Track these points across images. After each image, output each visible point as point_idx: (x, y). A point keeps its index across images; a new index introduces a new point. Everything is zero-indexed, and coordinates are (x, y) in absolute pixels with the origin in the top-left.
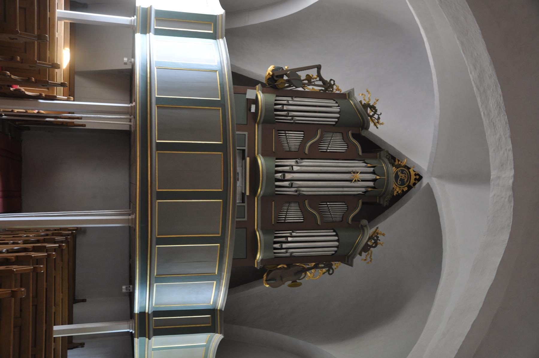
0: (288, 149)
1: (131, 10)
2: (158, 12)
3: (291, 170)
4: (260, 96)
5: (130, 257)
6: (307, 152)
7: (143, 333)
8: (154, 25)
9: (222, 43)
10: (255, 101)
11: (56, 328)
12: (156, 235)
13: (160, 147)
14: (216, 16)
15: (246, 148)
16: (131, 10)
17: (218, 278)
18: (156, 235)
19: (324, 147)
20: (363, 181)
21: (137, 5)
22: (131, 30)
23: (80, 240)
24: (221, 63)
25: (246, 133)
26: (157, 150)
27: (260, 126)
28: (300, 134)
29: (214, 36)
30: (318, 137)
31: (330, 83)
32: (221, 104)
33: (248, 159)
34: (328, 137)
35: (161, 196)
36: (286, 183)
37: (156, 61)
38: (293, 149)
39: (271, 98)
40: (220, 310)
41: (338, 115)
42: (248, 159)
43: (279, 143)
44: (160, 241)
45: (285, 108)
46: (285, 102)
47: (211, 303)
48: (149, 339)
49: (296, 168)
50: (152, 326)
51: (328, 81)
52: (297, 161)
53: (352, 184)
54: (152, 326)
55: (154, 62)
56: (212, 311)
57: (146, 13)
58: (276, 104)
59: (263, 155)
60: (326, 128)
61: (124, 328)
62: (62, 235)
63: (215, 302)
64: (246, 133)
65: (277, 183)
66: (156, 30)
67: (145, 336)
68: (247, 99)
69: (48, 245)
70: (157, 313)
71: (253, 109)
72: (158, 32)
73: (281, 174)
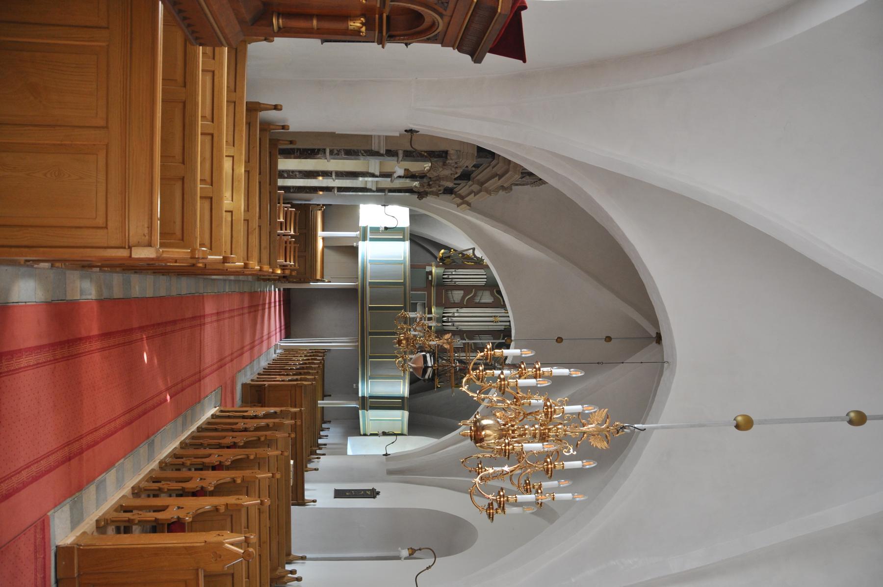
0: (453, 302)
1: (355, 227)
2: (371, 228)
3: (453, 315)
4: (434, 270)
5: (260, 519)
6: (465, 303)
7: (364, 407)
8: (369, 236)
9: (407, 244)
10: (430, 273)
11: (319, 402)
12: (369, 354)
13: (371, 308)
14: (404, 228)
15: (426, 302)
16: (355, 227)
17: (404, 378)
18: (369, 354)
19: (477, 300)
20: (500, 322)
21: (360, 225)
22: (356, 239)
23: (327, 353)
24: (405, 258)
25: (426, 293)
26: (369, 310)
27: (435, 288)
28: (461, 293)
29: (403, 240)
30: (473, 293)
31: (481, 259)
32: (404, 284)
33: (427, 309)
34: (480, 293)
35: (371, 334)
36: (450, 324)
37: (369, 260)
38: (456, 302)
39: (441, 271)
40: (407, 398)
41: (486, 280)
42: (427, 309)
43: (447, 298)
44: (371, 357)
45: (451, 277)
46: (450, 273)
47: (401, 393)
48: (367, 411)
49: (456, 315)
50: (369, 404)
51: (480, 257)
52: (458, 310)
53: (495, 324)
54: (369, 404)
55: (368, 262)
56: (402, 398)
57: (365, 229)
58: (444, 275)
59: (436, 306)
60: (478, 288)
61: (353, 405)
62: (321, 353)
63: (404, 392)
64: (426, 293)
65: (444, 324)
66: (370, 238)
67: (364, 409)
68: (427, 272)
69: (315, 362)
70: (371, 397)
71: (430, 278)
72: (372, 240)
73: (446, 318)
